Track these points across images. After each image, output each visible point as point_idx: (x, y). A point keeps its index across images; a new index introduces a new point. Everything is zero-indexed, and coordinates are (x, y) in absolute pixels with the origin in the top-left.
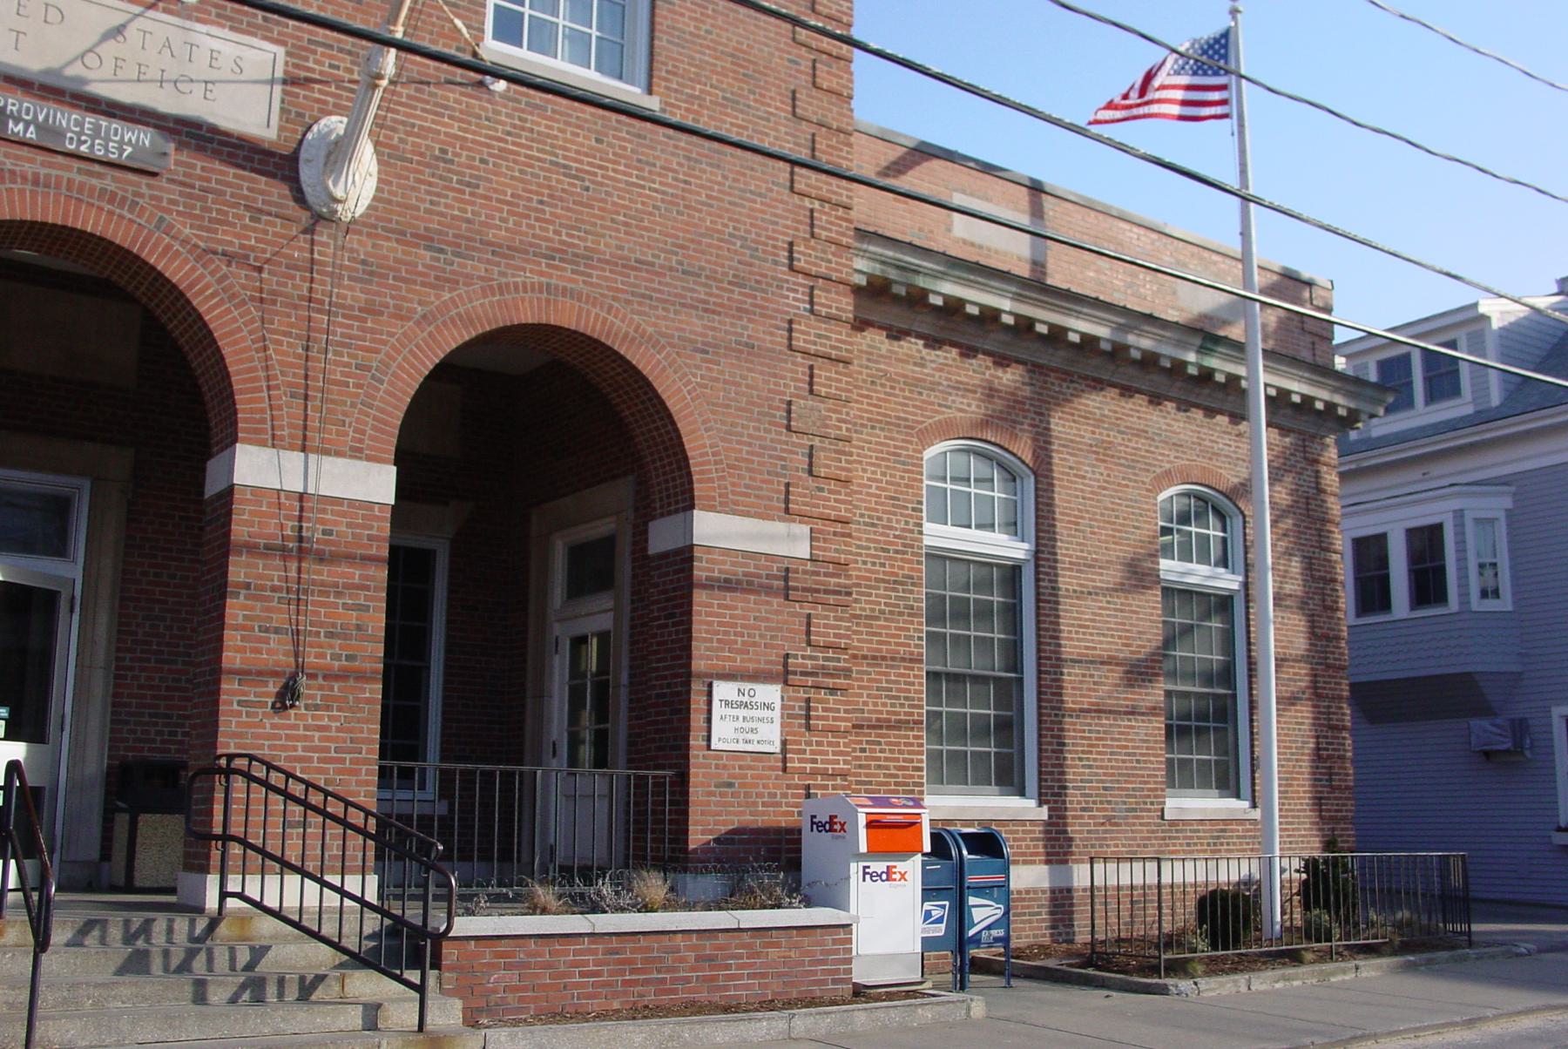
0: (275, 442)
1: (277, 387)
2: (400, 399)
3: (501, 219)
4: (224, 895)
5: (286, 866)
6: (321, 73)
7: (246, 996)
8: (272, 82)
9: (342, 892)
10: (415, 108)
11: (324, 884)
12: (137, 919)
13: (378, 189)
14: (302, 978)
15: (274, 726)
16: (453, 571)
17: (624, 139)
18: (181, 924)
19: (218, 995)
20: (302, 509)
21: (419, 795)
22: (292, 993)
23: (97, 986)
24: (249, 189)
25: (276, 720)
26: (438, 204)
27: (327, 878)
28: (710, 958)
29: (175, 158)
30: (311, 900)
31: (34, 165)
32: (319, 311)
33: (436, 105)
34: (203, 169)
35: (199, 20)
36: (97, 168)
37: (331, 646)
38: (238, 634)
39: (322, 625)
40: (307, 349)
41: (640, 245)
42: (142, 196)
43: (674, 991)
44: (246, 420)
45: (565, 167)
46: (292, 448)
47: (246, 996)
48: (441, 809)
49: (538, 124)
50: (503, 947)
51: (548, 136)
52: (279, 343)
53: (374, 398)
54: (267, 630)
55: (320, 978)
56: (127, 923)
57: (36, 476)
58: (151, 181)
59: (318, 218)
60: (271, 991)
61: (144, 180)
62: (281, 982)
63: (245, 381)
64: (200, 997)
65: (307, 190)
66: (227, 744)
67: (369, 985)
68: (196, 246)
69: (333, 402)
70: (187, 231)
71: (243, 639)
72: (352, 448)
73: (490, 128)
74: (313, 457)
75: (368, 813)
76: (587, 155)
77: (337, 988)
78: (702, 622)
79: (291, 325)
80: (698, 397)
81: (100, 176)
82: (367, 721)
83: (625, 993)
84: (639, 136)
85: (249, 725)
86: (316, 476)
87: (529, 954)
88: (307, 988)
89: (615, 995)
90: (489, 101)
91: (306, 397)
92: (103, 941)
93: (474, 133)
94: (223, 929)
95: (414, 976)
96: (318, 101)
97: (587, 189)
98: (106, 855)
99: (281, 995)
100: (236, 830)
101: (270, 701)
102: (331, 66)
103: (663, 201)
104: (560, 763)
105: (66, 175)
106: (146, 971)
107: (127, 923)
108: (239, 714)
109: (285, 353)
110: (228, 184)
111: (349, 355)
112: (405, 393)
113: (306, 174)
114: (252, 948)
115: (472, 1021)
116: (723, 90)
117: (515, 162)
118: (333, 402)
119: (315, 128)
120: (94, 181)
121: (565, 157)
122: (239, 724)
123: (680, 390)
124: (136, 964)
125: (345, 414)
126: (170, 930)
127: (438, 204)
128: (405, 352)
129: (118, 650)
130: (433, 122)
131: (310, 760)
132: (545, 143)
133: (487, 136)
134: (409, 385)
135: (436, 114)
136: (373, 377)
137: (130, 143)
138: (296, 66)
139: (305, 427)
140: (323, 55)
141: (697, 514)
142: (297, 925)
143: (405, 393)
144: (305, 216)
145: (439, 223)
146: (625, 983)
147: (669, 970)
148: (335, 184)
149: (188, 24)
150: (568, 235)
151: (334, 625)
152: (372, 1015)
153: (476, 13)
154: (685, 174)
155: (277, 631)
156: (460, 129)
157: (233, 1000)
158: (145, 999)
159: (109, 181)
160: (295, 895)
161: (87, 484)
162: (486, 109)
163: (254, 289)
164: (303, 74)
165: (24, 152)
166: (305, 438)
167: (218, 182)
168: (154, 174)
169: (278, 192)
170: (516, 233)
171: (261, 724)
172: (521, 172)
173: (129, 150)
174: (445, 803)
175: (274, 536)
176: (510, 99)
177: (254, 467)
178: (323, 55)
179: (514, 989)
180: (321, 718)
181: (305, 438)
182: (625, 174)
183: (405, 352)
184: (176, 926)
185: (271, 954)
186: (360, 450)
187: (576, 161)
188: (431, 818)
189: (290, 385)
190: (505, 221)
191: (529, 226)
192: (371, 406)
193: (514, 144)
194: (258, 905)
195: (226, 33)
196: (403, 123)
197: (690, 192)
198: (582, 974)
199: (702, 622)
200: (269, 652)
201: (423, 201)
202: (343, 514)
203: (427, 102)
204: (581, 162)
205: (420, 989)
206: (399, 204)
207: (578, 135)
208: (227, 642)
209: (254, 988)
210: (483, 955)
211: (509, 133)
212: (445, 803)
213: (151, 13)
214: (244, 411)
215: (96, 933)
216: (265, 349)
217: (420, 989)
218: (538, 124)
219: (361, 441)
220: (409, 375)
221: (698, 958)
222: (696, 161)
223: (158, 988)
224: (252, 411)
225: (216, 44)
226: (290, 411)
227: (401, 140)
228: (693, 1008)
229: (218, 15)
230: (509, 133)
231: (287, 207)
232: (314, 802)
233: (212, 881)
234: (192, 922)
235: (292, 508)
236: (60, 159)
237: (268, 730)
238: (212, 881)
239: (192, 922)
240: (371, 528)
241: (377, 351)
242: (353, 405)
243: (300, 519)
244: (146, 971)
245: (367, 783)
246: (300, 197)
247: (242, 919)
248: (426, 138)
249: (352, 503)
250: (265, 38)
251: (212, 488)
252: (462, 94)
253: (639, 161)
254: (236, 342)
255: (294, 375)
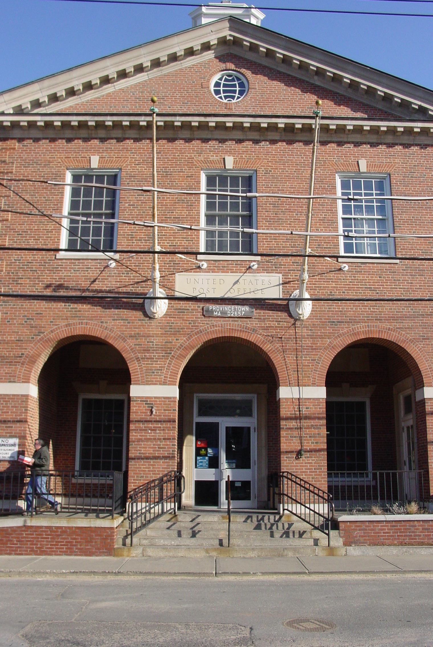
0: (290, 385)
1: (289, 370)
2: (325, 368)
3: (351, 309)
4: (284, 510)
5: (297, 502)
6: (293, 278)
7: (285, 536)
8: (279, 285)
9: (309, 508)
10: (321, 282)
11: (306, 507)
12: (260, 516)
13: (312, 308)
14: (299, 532)
15: (296, 463)
16: (371, 408)
17: (388, 275)
18: (272, 517)
19: (277, 535)
20: (299, 403)
21: (366, 479)
22: (297, 535)
23: (247, 532)
24: (276, 316)
25: (297, 462)
26: (331, 308)
27: (306, 505)
28: (427, 529)
29: (256, 313)
30: (303, 512)
31: (221, 322)
32: (299, 346)
33: (327, 279)
34: (263, 313)
35: (258, 273)
36: (236, 319)
37: (311, 440)
38: (284, 439)
39: (308, 434)
40: (297, 357)
41: (397, 306)
42: (248, 324)
43: (416, 539)
44: (282, 380)
45: (370, 288)
46: (295, 386)
47: (285, 536)
48: (373, 483)
49: (360, 277)
50: (358, 524)
51: (363, 280)
52: (289, 357)
53: (317, 368)
54: (292, 437)
55: (304, 532)
56: (258, 517)
57: (244, 395)
58: (250, 319)
59: (296, 320)
60: (291, 535)
61: (248, 320)
62: (294, 532)
63: (280, 369)
64: (272, 535)
65: (292, 313)
66: (284, 469)
67: (317, 534)
68: (263, 335)
69: (305, 371)
70: (261, 331)
71: (286, 440)
72: (312, 384)
73: (344, 282)
74: (301, 388)
75: (324, 492)
76: (376, 283)
77: (310, 534)
78: (429, 423)
79: (292, 352)
80: (422, 351)
81: (237, 321)
82: (323, 460)
83: (399, 539)
84: (394, 272)
85: (289, 463)
86: (304, 393)
87: (366, 526)
88: (301, 535)
89: (395, 539)
90: (343, 274)
91: (298, 371)
92: (252, 521)
93: (340, 285)
94: (283, 519)
95: (327, 532)
96: (292, 287)
97: (378, 293)
98: (269, 500)
99: (294, 536)
100: (285, 493)
101: (295, 456)
102: (295, 276)
103: (404, 291)
104: (406, 468)
105: (229, 323)
106: (260, 529)
107: (258, 517)
108: (286, 460)
109: (290, 360)
110: (270, 316)
111: (309, 357)
112: (326, 365)
113: (291, 308)
114: (289, 524)
115: (346, 544)
116: (422, 250)
117: (353, 290)
118: (305, 371)
119: (292, 295)
120: (236, 323)
121: (369, 285)
122: (286, 463)
123: (416, 350)
124: (258, 527)
125: (309, 374)
126: (269, 519)
127: (331, 308)
128: (325, 353)
129: (268, 441)
130: (327, 284)
131: (307, 472)
132: (362, 282)
133: (344, 285)
134: (327, 363)
135: (328, 282)
136: (317, 362)
137: (243, 311)
138: (285, 278)
139: (298, 379)
140: (292, 273)
141: (425, 388)
142: (300, 517)
143: (326, 365)
144: (292, 321)
145: (332, 314)
146: (398, 536)
147: (413, 532)
148: (299, 310)
149: (255, 274)
150: (373, 309)
151: (311, 434)
152: (316, 542)
153: (337, 248)
154: (411, 280)
155: (295, 437)
156: (335, 284)
157: (281, 537)
158: (259, 535)
159: (240, 322)
160: (303, 509)
161: (256, 395)
162: (343, 277)
163: (280, 343)
164: (287, 280)
165: (218, 319)
166: (298, 382)
167: (268, 316)
168: (251, 318)
169: (284, 315)
170: (356, 312)
171: (293, 463)
172: (355, 293)
173: (243, 312)
174: (374, 481)
175: (292, 411)
176: (350, 272)
177: (285, 392)
178: (292, 273)
179: (362, 536)
180: (309, 460)
181: (298, 382)
182: (390, 285)
183: (325, 353)
184: (270, 518)
185: (294, 525)
186: (315, 384)
187: (373, 285)
188: (345, 486)
189: (293, 368)
190: (353, 309)
191: (360, 309)
192: (317, 371)
193: (352, 285)
194: (291, 512)
195: (265, 274)
196: (318, 287)
197: (413, 286)
198: (384, 533)
199: (429, 423)
200: (294, 443)
201: (327, 308)
202: (311, 403)
203: (324, 279)
204: (375, 285)
205: (328, 535)
206: (319, 311)
207: (373, 277)
208: (282, 441)
209: (286, 534)
210: (352, 526)
211: (351, 282)
212: (374, 481)
213: (245, 274)
214: (281, 377)
215: (250, 519)
216: (285, 359)
217: (328, 535)
218: (360, 277)
219: (315, 381)
220: (327, 360)
221: (423, 529)
222: (414, 275)
223: (264, 533)
224: (283, 377)
225: (263, 278)
226: (293, 376)
227: (318, 292)
228: (422, 544)
229: (263, 270)
230: (351, 282)
231: (287, 319)
232: (304, 485)
233: (281, 505)
234: (275, 517)
235: (296, 402)
236: (227, 319)
237: (295, 464)
238: (281, 505)
239: (275, 517)
240: (320, 405)
241: (317, 355)
242: (311, 371)
243: (299, 405)
244: (260, 529)
245: (324, 478)
246: (291, 316)
247: (288, 516)
248: (325, 290)
249: (314, 399)
250: (276, 273)
251: (277, 399)
252: (335, 274)
253: (394, 280)
254: (277, 359)
255: (294, 365)
